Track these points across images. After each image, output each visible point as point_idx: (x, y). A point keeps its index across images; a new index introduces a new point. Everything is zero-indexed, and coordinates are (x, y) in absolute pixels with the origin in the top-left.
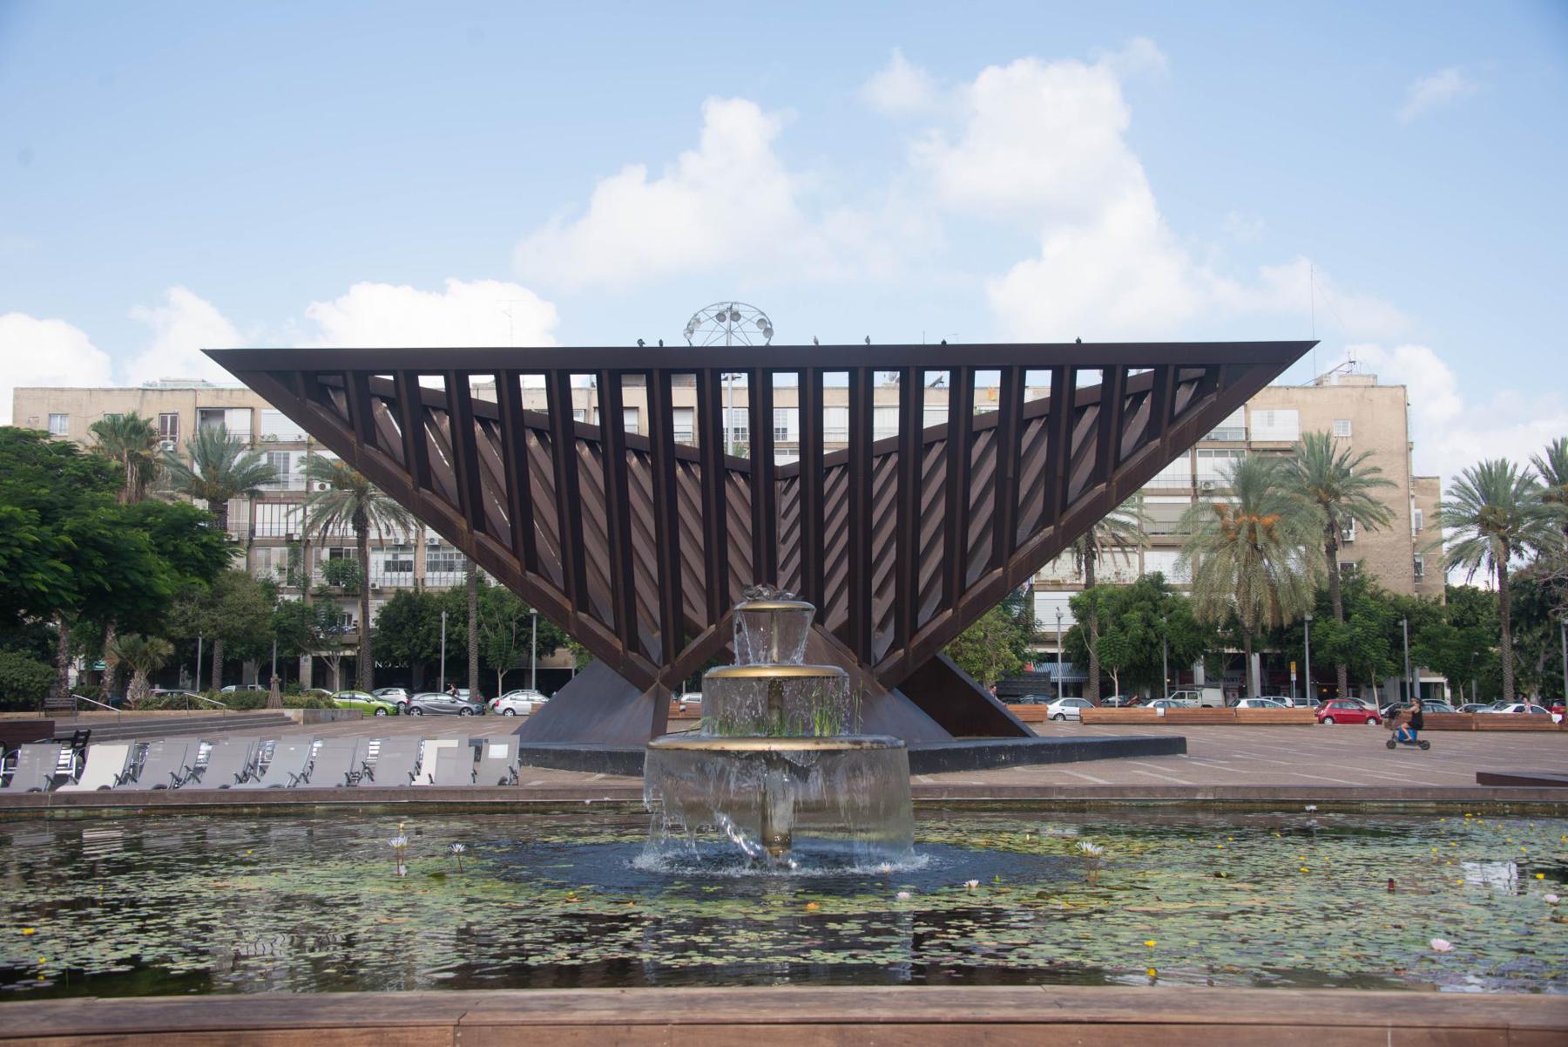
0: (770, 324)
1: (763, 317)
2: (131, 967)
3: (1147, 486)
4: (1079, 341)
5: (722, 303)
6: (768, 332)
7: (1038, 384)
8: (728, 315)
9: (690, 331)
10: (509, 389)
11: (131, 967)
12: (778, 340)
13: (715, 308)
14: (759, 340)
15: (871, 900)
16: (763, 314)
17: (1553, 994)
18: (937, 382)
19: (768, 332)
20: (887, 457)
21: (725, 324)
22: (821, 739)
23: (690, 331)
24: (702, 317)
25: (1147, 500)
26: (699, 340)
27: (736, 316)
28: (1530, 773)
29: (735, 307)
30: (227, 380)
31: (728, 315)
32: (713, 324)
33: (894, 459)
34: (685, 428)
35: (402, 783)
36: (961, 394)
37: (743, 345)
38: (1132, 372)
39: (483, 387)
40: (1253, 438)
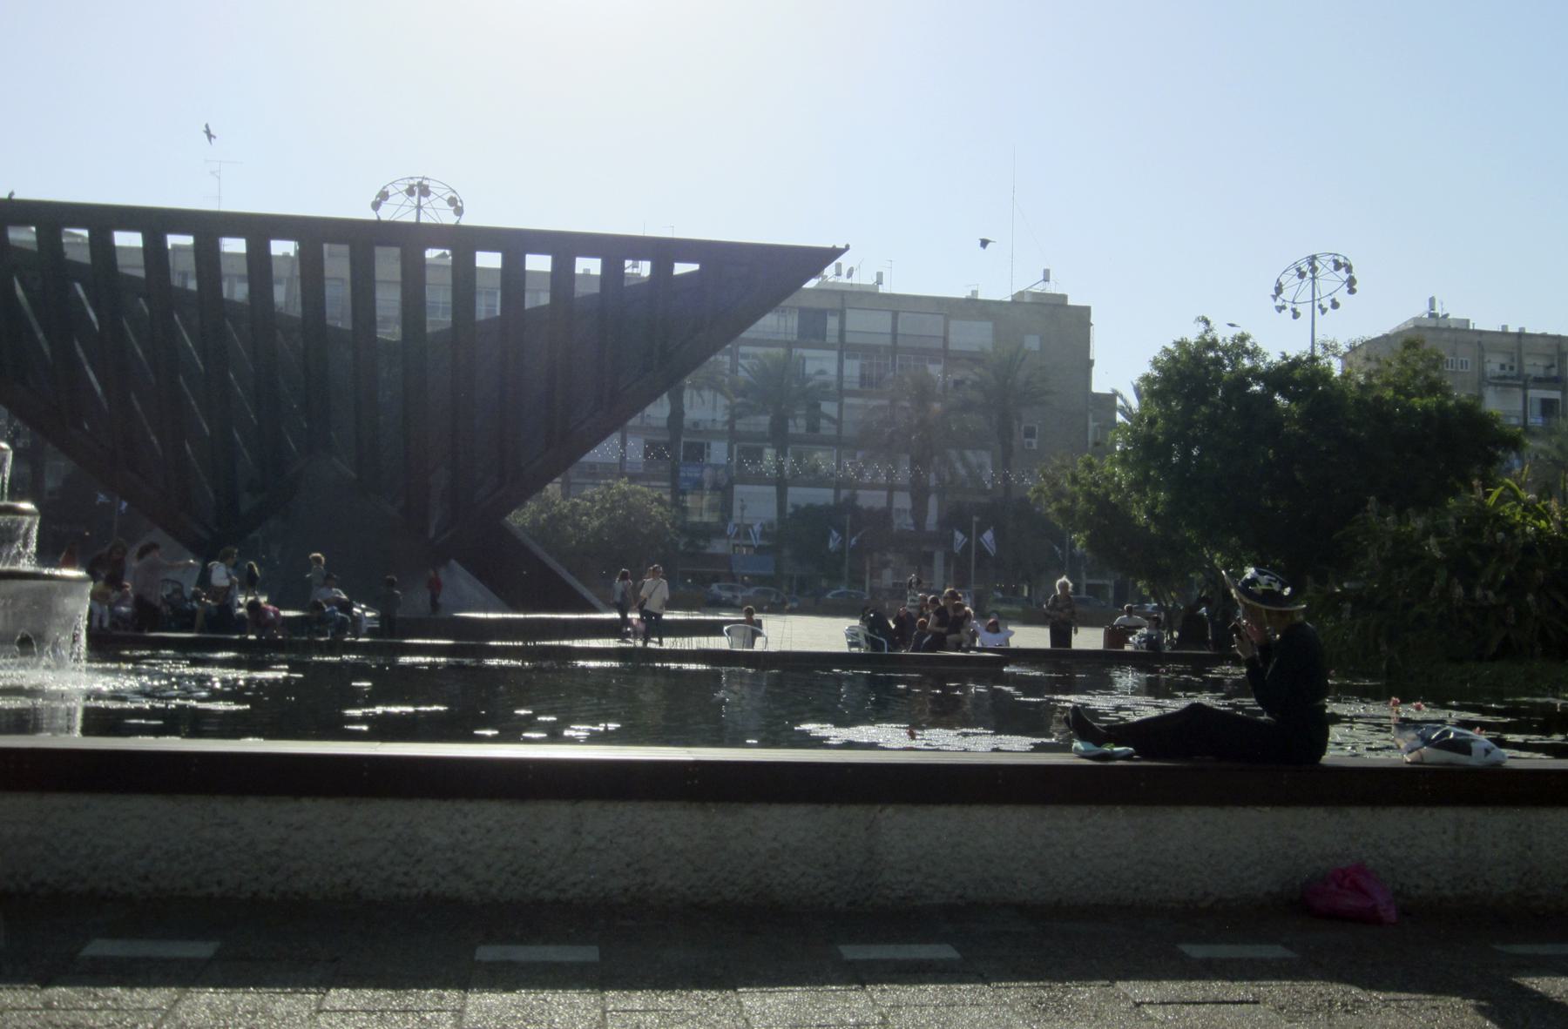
0: (461, 201)
1: (454, 195)
2: (446, 708)
3: (744, 335)
4: (1092, 325)
5: (412, 178)
6: (459, 211)
8: (417, 190)
9: (376, 206)
11: (446, 708)
12: (468, 220)
13: (406, 181)
14: (448, 218)
15: (1383, 755)
16: (454, 192)
17: (3, 675)
19: (459, 211)
21: (415, 199)
22: (875, 634)
23: (376, 206)
24: (391, 190)
25: (743, 349)
26: (387, 213)
27: (425, 191)
28: (21, 241)
29: (425, 182)
30: (1493, 745)
31: (417, 190)
32: (402, 198)
35: (1416, 314)
37: (434, 222)
40: (951, 347)
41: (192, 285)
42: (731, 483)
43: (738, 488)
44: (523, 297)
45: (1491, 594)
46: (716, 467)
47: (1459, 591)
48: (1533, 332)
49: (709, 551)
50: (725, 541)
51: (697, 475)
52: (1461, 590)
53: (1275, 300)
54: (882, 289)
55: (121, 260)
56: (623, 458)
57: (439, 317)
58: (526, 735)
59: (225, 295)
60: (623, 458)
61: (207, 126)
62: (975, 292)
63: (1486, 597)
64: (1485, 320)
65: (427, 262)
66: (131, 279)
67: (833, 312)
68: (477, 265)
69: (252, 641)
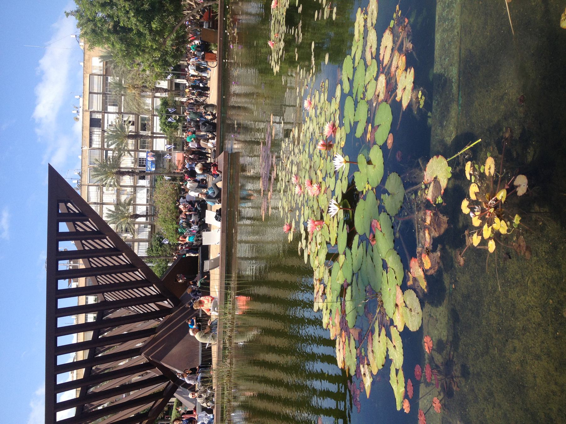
7: (63, 227)
20: (83, 244)
33: (91, 259)
34: (82, 355)
36: (66, 237)
38: (60, 212)
42: (152, 151)
43: (154, 149)
46: (147, 156)
67: (91, 115)
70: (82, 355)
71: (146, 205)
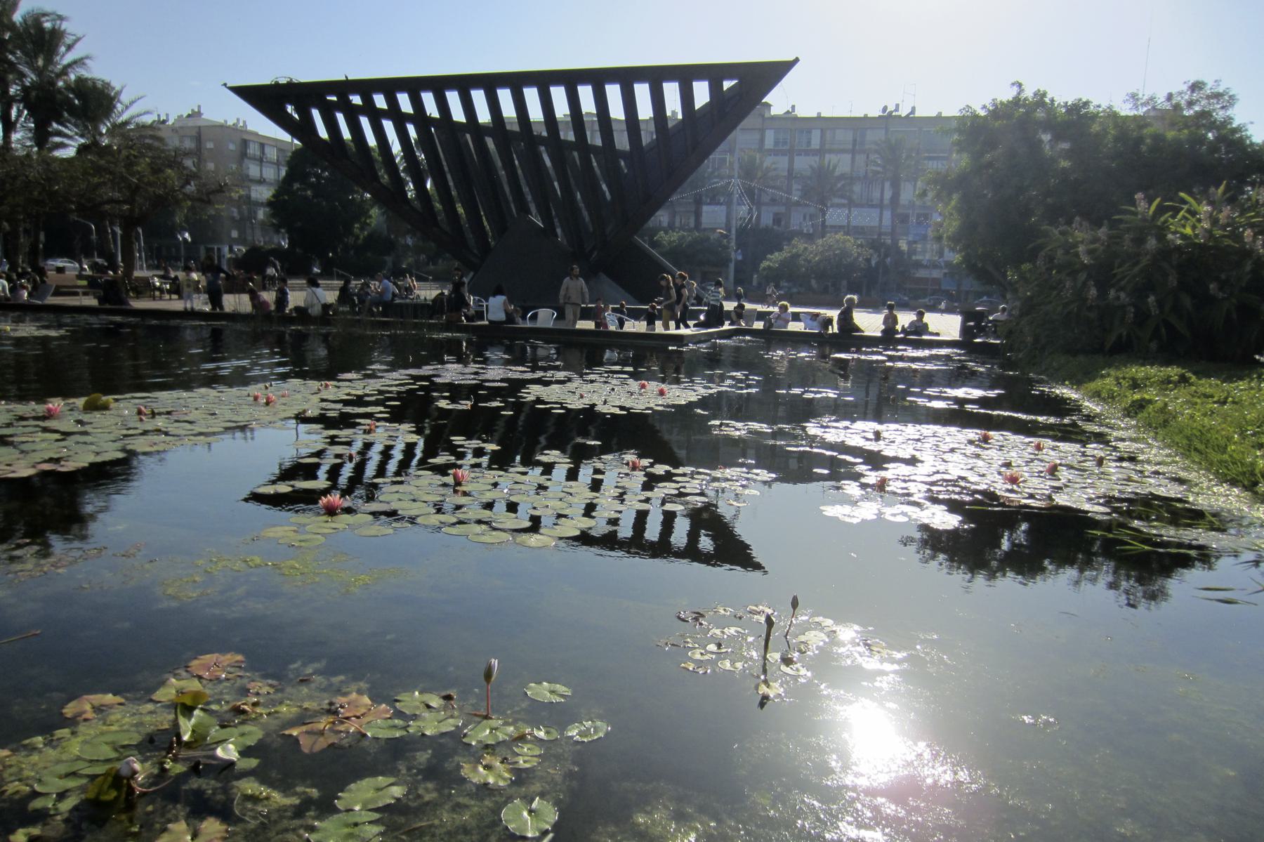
7: (702, 93)
10: (393, 102)
18: (671, 91)
34: (484, 116)
36: (687, 97)
39: (380, 101)
41: (545, 134)
44: (613, 135)
45: (1122, 295)
47: (1093, 292)
48: (802, 116)
49: (917, 275)
50: (938, 271)
51: (923, 232)
52: (1095, 292)
53: (982, 108)
54: (917, 115)
55: (534, 128)
56: (849, 222)
57: (622, 141)
58: (216, 262)
59: (589, 142)
60: (849, 222)
61: (125, 86)
62: (940, 113)
63: (1118, 298)
64: (925, 110)
65: (506, 121)
66: (513, 132)
68: (640, 118)
69: (191, 235)
70: (484, 116)
71: (848, 226)
